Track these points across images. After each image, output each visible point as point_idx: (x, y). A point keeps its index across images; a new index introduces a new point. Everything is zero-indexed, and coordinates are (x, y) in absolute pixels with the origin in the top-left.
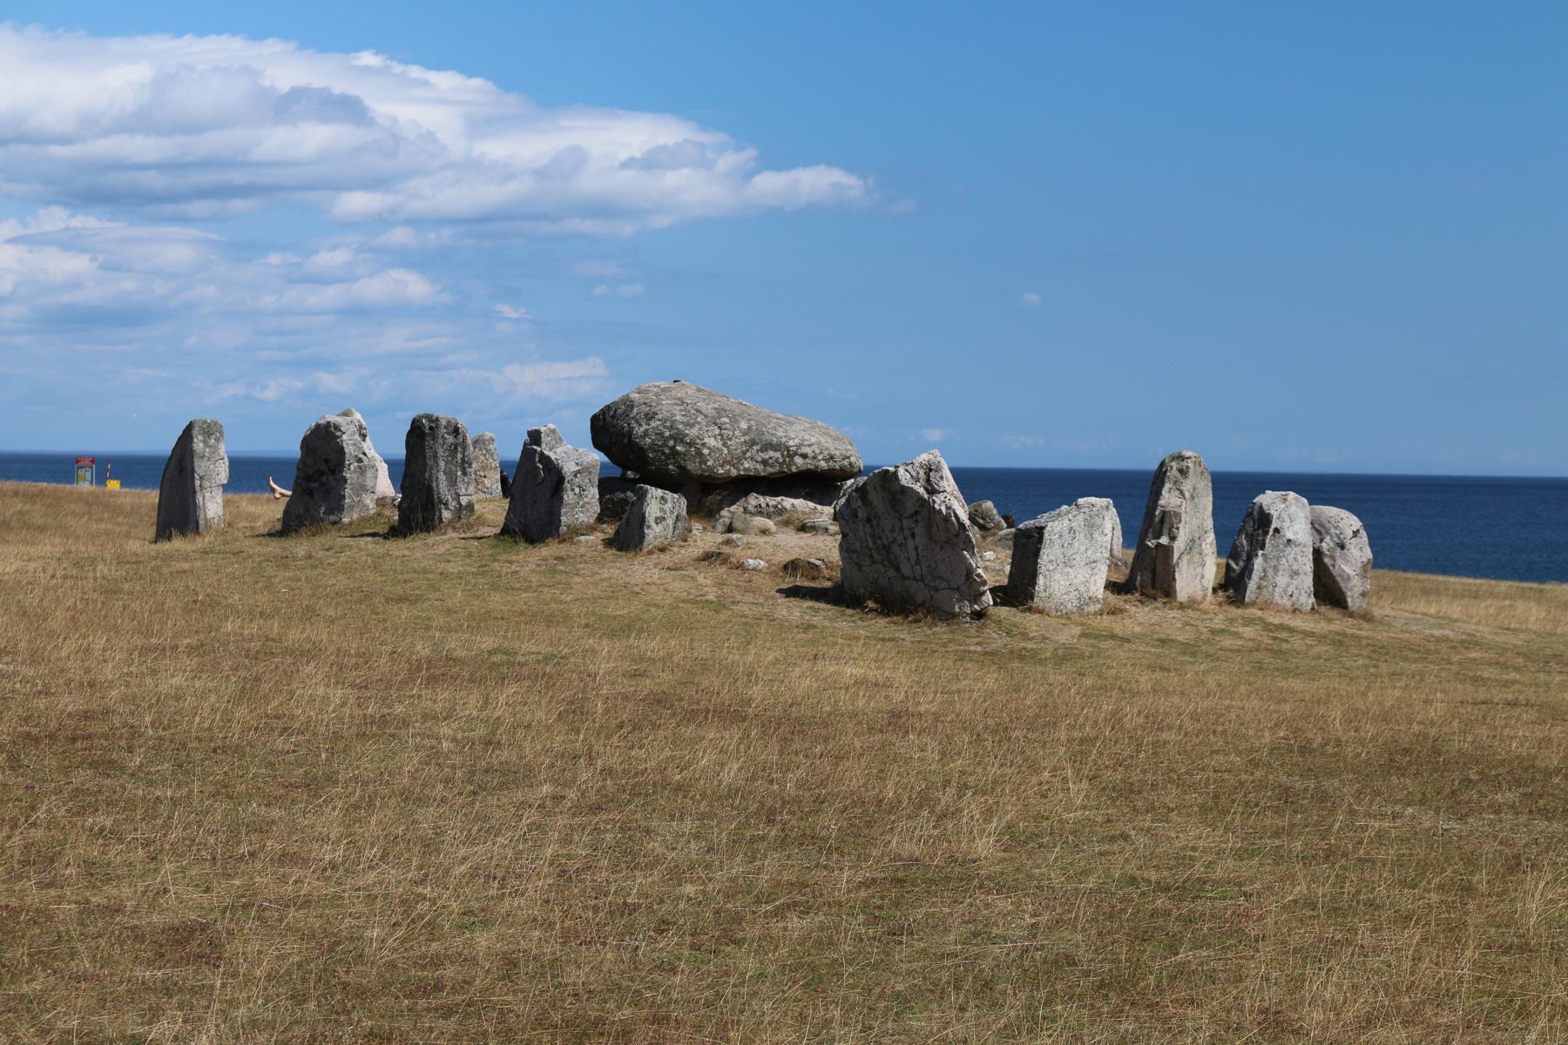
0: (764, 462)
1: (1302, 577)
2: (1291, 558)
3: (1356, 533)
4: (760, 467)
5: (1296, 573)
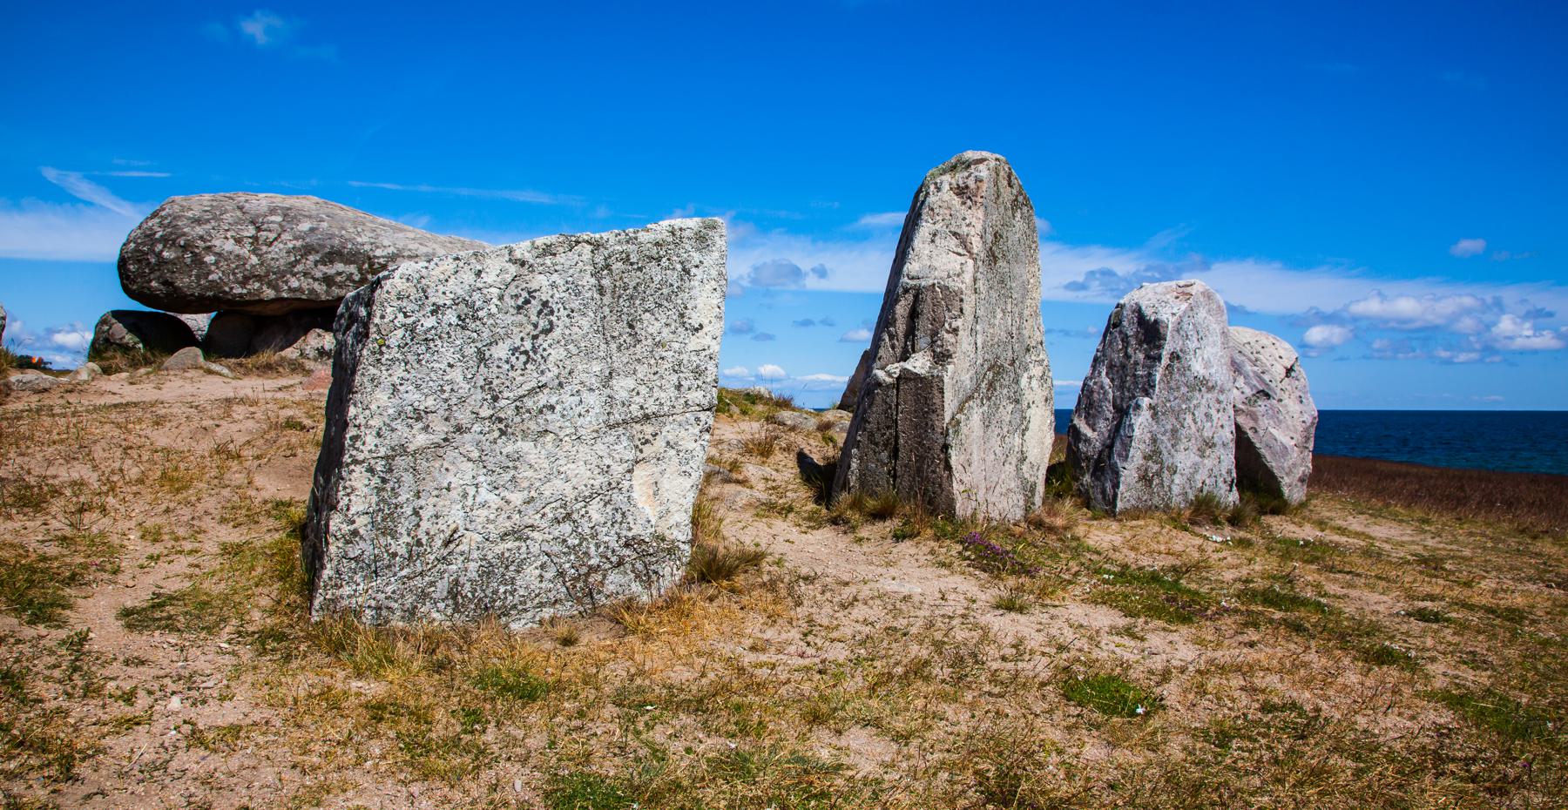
0: (328, 280)
1: (1219, 451)
2: (1200, 414)
4: (320, 288)
5: (1210, 444)
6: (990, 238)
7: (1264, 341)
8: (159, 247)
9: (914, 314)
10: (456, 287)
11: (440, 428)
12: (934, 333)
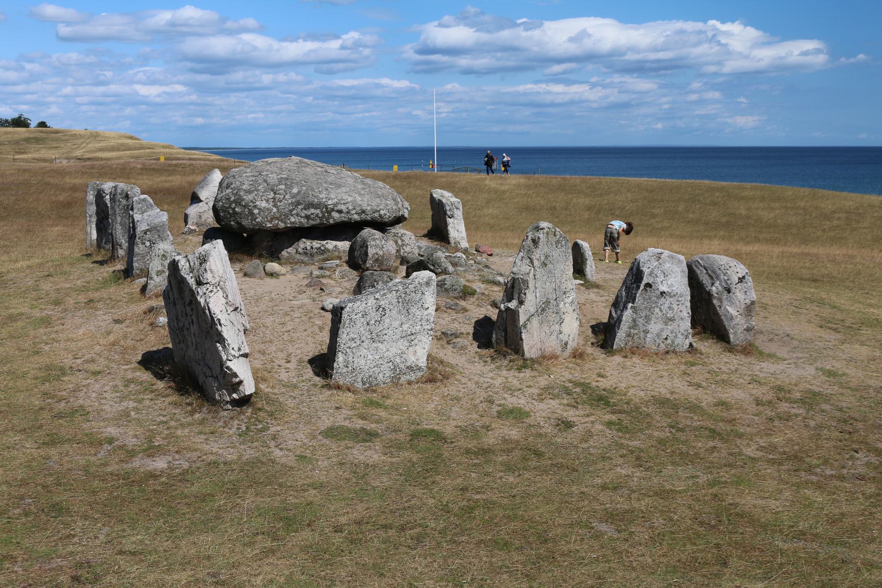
0: (307, 217)
2: (665, 307)
3: (741, 280)
4: (304, 221)
6: (543, 258)
7: (731, 264)
8: (233, 205)
10: (361, 308)
11: (358, 342)
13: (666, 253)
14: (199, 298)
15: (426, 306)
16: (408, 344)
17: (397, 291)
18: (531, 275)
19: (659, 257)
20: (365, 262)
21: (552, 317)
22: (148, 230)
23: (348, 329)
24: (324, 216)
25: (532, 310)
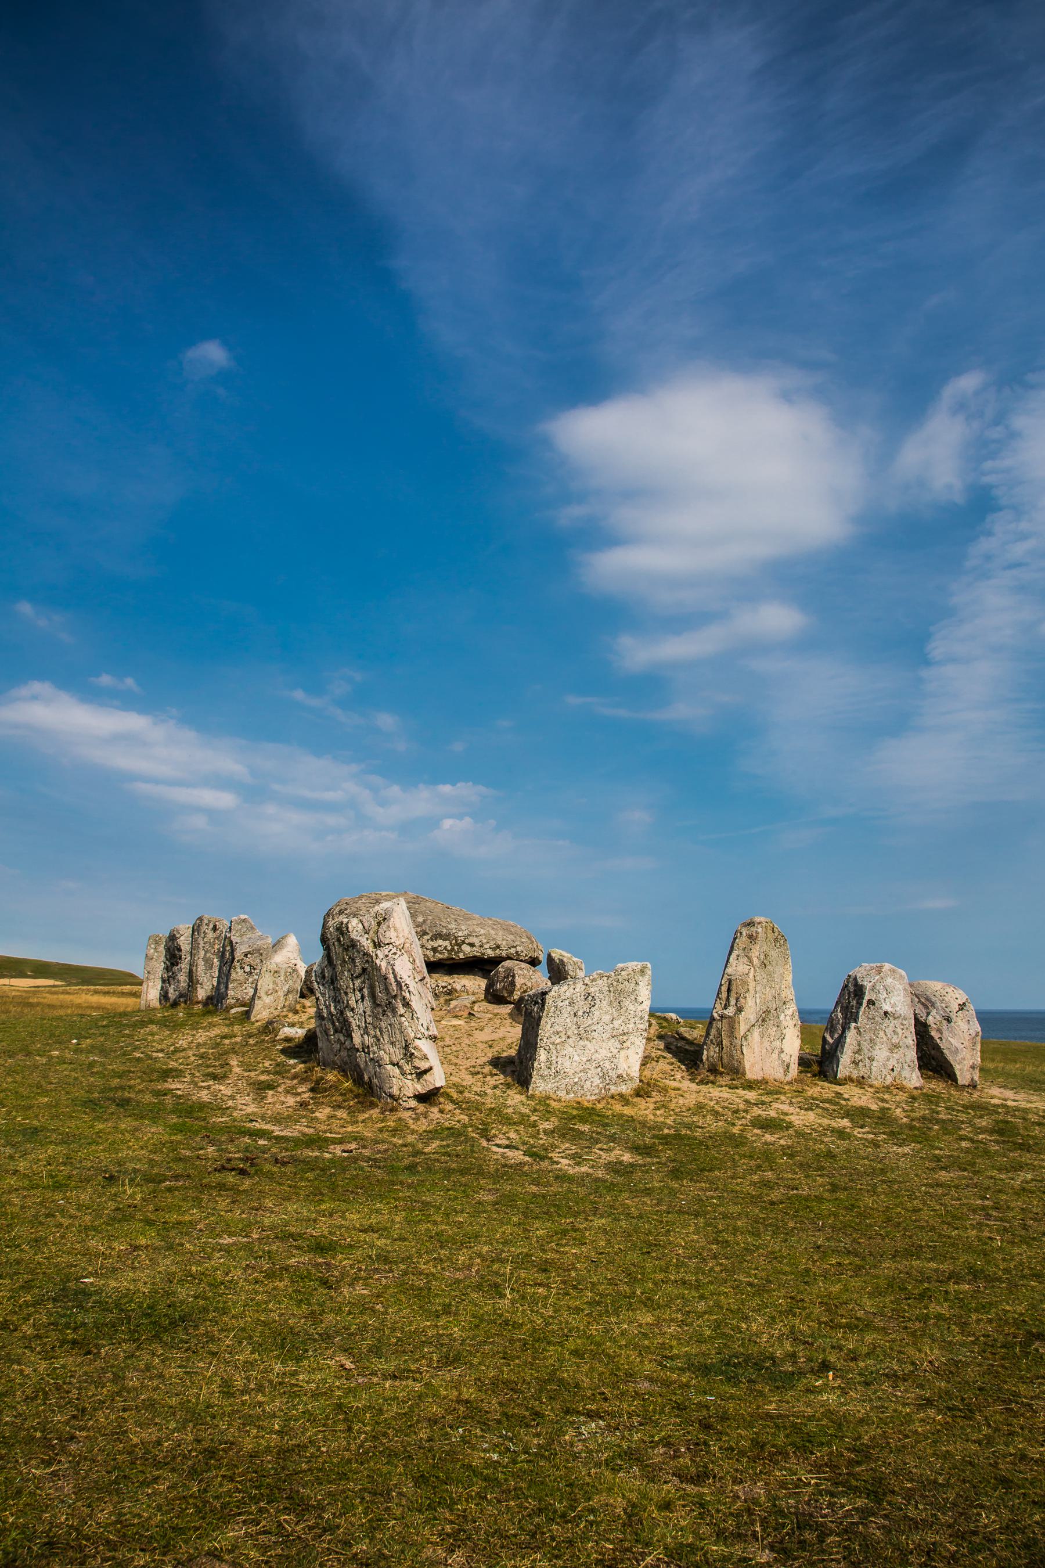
0: (434, 950)
2: (889, 1031)
3: (962, 1007)
6: (762, 957)
9: (729, 991)
12: (737, 999)
13: (887, 966)
14: (378, 962)
15: (640, 999)
16: (619, 1046)
17: (609, 977)
18: (751, 975)
19: (879, 971)
20: (511, 993)
21: (773, 1031)
22: (249, 952)
23: (553, 1019)
24: (453, 949)
25: (753, 1020)
